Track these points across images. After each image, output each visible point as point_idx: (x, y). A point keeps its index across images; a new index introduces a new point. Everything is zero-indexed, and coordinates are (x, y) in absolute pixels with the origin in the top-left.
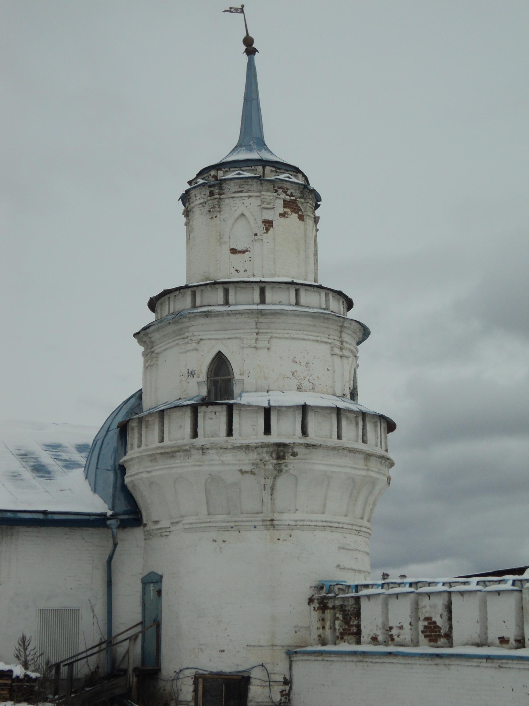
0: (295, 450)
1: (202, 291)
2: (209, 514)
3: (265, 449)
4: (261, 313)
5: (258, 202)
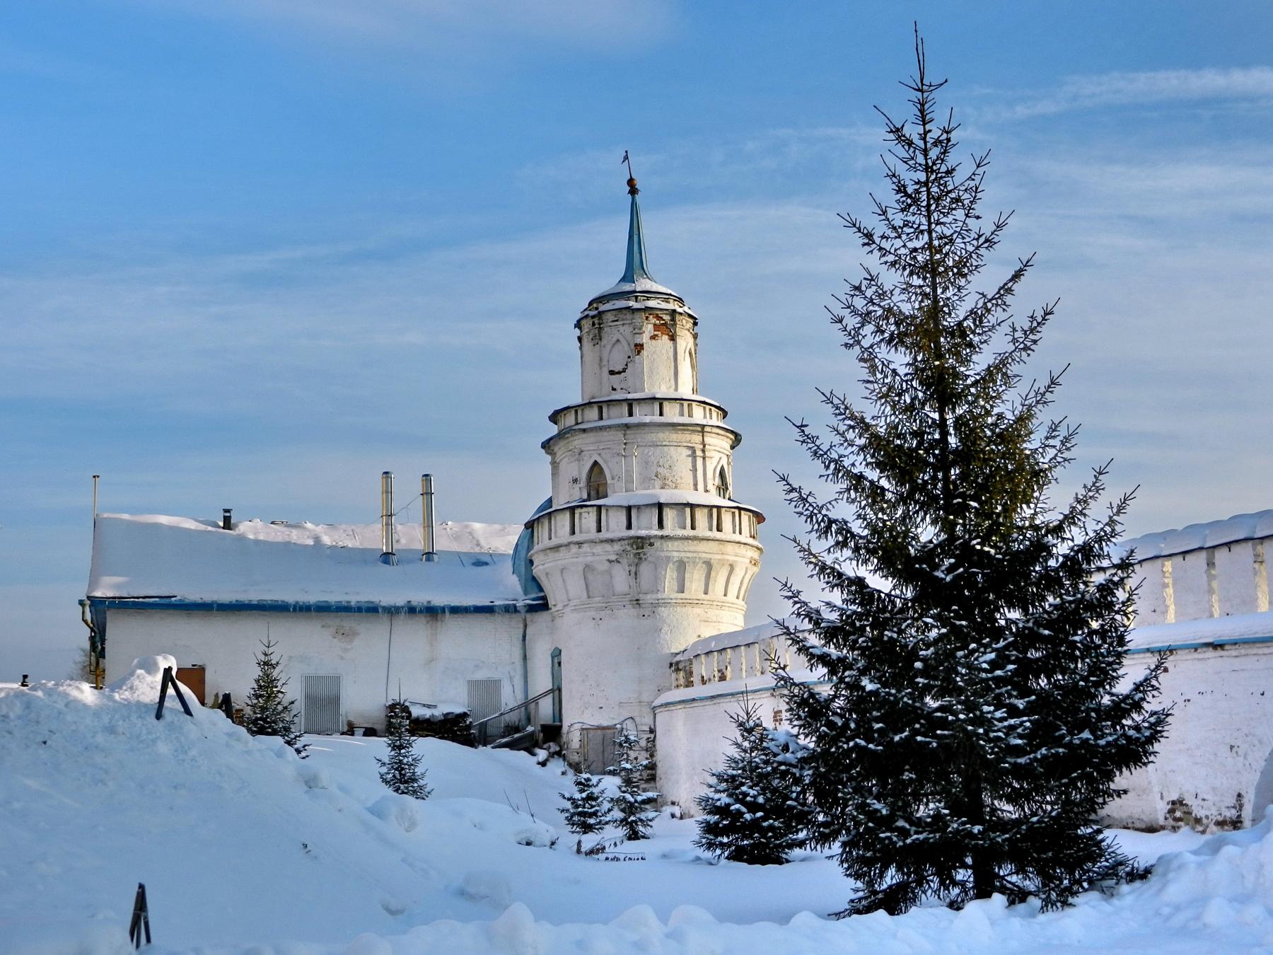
0: (652, 541)
1: (583, 410)
2: (589, 597)
3: (626, 542)
4: (627, 426)
5: (631, 329)
